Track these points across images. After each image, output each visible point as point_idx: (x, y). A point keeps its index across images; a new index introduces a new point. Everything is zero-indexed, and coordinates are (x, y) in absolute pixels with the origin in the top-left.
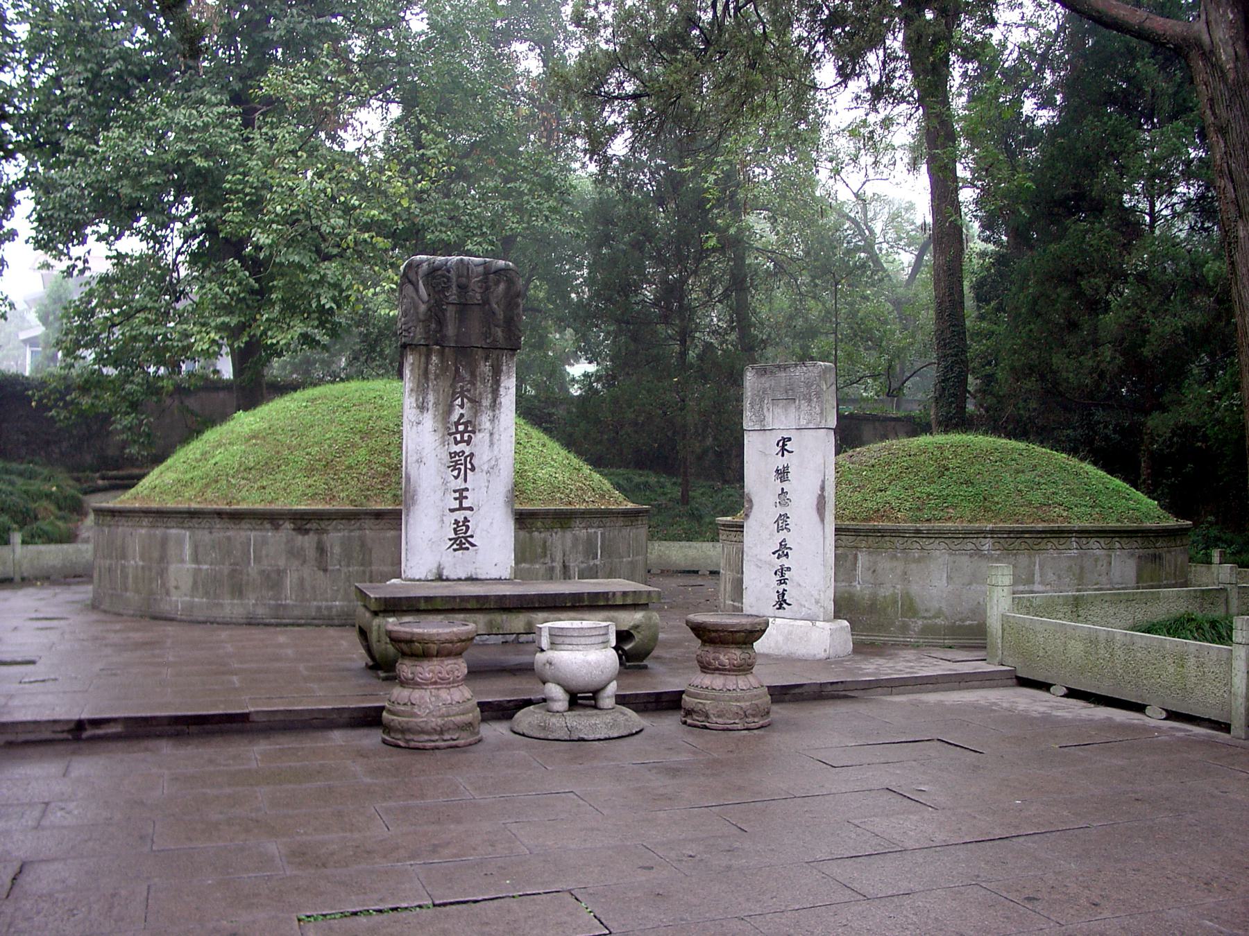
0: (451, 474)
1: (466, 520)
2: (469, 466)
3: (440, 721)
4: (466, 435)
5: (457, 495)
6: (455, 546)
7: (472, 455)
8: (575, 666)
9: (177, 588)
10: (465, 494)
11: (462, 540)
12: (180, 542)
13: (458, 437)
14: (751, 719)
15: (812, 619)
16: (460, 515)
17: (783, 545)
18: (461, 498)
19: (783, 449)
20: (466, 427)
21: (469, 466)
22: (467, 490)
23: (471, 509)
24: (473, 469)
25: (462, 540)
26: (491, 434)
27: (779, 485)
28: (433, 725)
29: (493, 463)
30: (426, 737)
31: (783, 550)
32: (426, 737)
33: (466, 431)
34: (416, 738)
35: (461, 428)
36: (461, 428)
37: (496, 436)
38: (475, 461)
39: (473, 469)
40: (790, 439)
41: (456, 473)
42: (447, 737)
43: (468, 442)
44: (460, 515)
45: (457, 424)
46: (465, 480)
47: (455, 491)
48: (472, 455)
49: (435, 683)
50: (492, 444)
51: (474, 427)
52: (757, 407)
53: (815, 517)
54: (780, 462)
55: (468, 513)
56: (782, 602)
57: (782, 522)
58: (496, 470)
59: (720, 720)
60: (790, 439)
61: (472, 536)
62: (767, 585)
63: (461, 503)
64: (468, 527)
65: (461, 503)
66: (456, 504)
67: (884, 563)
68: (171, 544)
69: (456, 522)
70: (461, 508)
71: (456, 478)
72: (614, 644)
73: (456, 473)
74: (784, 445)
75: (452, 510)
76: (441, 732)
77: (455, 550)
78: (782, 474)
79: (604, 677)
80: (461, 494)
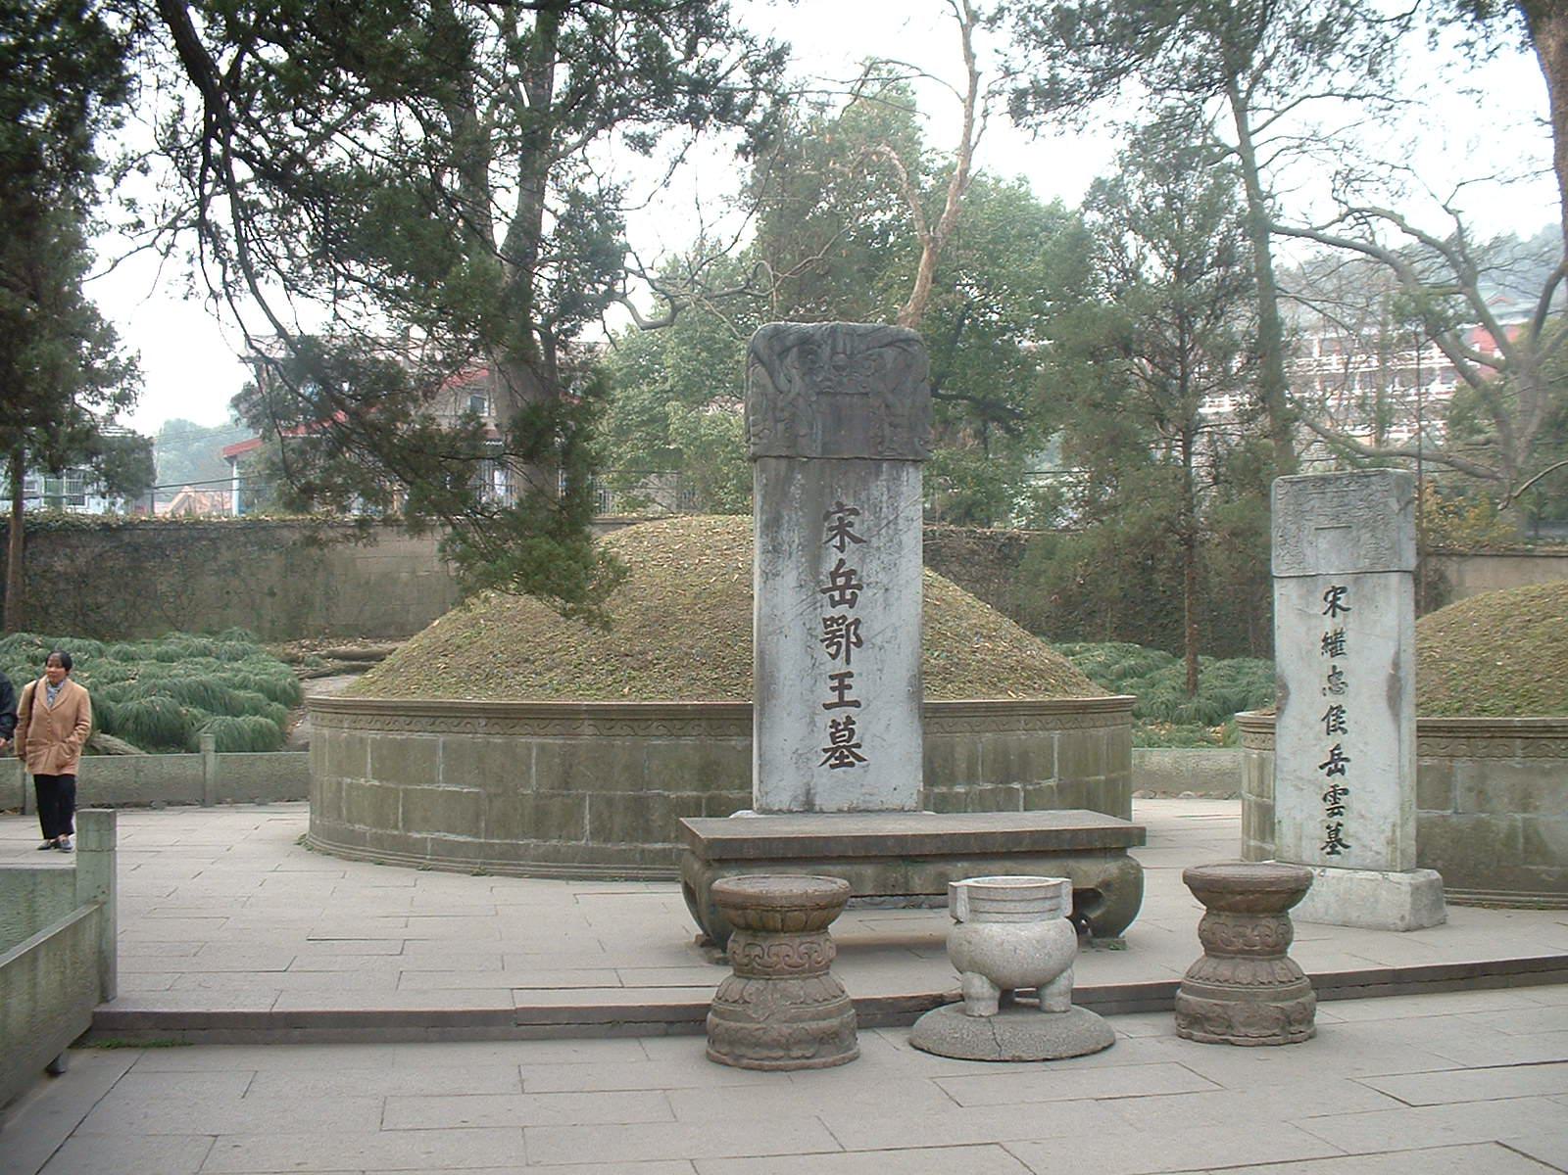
0: (823, 652)
1: (849, 721)
2: (853, 639)
3: (786, 1029)
5: (836, 683)
6: (833, 761)
7: (857, 622)
10: (847, 681)
11: (843, 752)
13: (837, 595)
16: (840, 715)
18: (842, 688)
19: (1334, 605)
21: (853, 639)
22: (850, 675)
23: (856, 704)
27: (1327, 662)
28: (775, 1034)
30: (765, 1053)
31: (1336, 763)
33: (848, 586)
34: (750, 1053)
35: (841, 581)
36: (841, 581)
39: (859, 643)
40: (1343, 590)
41: (833, 650)
42: (796, 1052)
43: (852, 603)
44: (840, 715)
45: (834, 575)
46: (848, 661)
47: (832, 677)
48: (857, 622)
54: (1328, 625)
55: (852, 711)
57: (1335, 719)
59: (1252, 1032)
61: (858, 746)
64: (852, 732)
66: (834, 698)
70: (842, 703)
71: (834, 657)
73: (833, 650)
74: (1336, 599)
75: (827, 707)
76: (787, 1048)
78: (1333, 644)
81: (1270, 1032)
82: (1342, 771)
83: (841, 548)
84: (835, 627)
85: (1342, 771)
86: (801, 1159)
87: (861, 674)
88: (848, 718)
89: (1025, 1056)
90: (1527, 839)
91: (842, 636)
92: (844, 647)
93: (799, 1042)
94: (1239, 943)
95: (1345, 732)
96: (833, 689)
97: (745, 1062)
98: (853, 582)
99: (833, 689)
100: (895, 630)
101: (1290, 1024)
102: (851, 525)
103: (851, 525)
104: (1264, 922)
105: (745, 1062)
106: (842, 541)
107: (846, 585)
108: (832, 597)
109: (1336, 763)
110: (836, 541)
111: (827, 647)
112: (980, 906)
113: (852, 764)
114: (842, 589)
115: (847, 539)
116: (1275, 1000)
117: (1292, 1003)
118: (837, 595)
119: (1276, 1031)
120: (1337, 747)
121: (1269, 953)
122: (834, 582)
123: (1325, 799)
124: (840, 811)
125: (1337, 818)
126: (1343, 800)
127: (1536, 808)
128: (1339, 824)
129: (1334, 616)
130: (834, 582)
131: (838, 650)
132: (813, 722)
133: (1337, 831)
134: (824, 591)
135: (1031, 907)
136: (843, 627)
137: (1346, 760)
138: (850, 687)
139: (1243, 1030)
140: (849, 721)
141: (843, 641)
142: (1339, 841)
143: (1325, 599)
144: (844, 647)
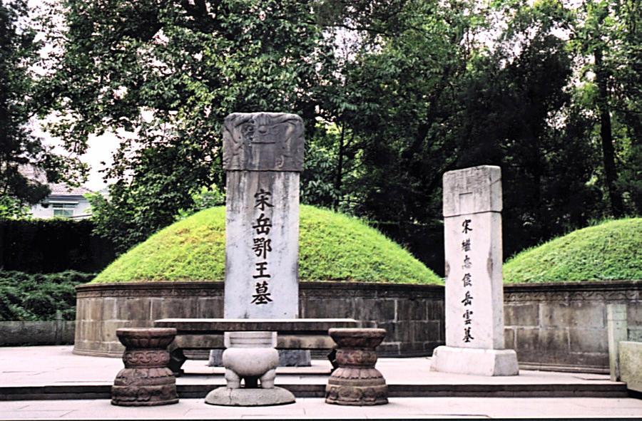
0: (254, 254)
1: (265, 283)
2: (267, 248)
3: (136, 388)
5: (259, 267)
6: (257, 301)
7: (269, 241)
8: (245, 361)
9: (108, 335)
10: (264, 266)
11: (262, 296)
12: (112, 306)
13: (260, 229)
14: (368, 399)
15: (485, 348)
16: (261, 281)
17: (468, 296)
18: (262, 269)
19: (466, 228)
20: (266, 222)
21: (267, 248)
22: (266, 263)
23: (268, 276)
24: (270, 250)
25: (262, 296)
26: (283, 227)
27: (465, 253)
28: (131, 390)
29: (283, 246)
30: (127, 399)
31: (467, 300)
32: (127, 399)
33: (265, 225)
34: (122, 399)
35: (262, 223)
36: (262, 223)
37: (285, 228)
38: (271, 245)
39: (270, 250)
40: (470, 221)
41: (258, 252)
42: (140, 399)
43: (267, 232)
44: (261, 281)
45: (259, 220)
46: (265, 257)
47: (258, 264)
48: (269, 241)
50: (283, 233)
51: (271, 222)
52: (451, 200)
53: (486, 274)
54: (465, 237)
56: (468, 337)
57: (467, 279)
58: (285, 251)
59: (345, 399)
60: (470, 221)
61: (269, 294)
62: (459, 325)
63: (261, 272)
64: (266, 289)
65: (261, 272)
66: (258, 273)
67: (558, 312)
68: (106, 307)
69: (258, 285)
70: (262, 276)
71: (259, 255)
72: (275, 345)
73: (258, 252)
74: (467, 225)
75: (255, 277)
76: (137, 396)
77: (257, 303)
78: (466, 245)
79: (262, 367)
80: (262, 267)
82: (470, 303)
83: (263, 209)
84: (259, 243)
85: (470, 303)
86: (46, 412)
87: (270, 263)
89: (240, 404)
90: (572, 338)
92: (263, 252)
93: (142, 394)
94: (346, 360)
95: (471, 285)
96: (258, 269)
97: (120, 403)
98: (268, 223)
99: (258, 269)
100: (286, 244)
101: (366, 397)
102: (267, 199)
103: (267, 199)
104: (357, 351)
105: (120, 403)
106: (263, 206)
107: (264, 225)
108: (258, 230)
109: (467, 300)
110: (260, 206)
112: (234, 341)
113: (266, 303)
114: (263, 226)
115: (265, 205)
116: (357, 385)
117: (366, 387)
118: (260, 229)
119: (358, 399)
120: (468, 292)
121: (359, 365)
122: (259, 223)
123: (464, 316)
124: (464, 374)
125: (469, 325)
126: (471, 317)
127: (576, 324)
128: (469, 328)
130: (259, 223)
132: (248, 284)
133: (469, 331)
134: (254, 227)
135: (254, 341)
137: (472, 298)
138: (265, 269)
139: (342, 398)
140: (265, 283)
141: (263, 249)
142: (469, 336)
143: (463, 225)
144: (263, 252)
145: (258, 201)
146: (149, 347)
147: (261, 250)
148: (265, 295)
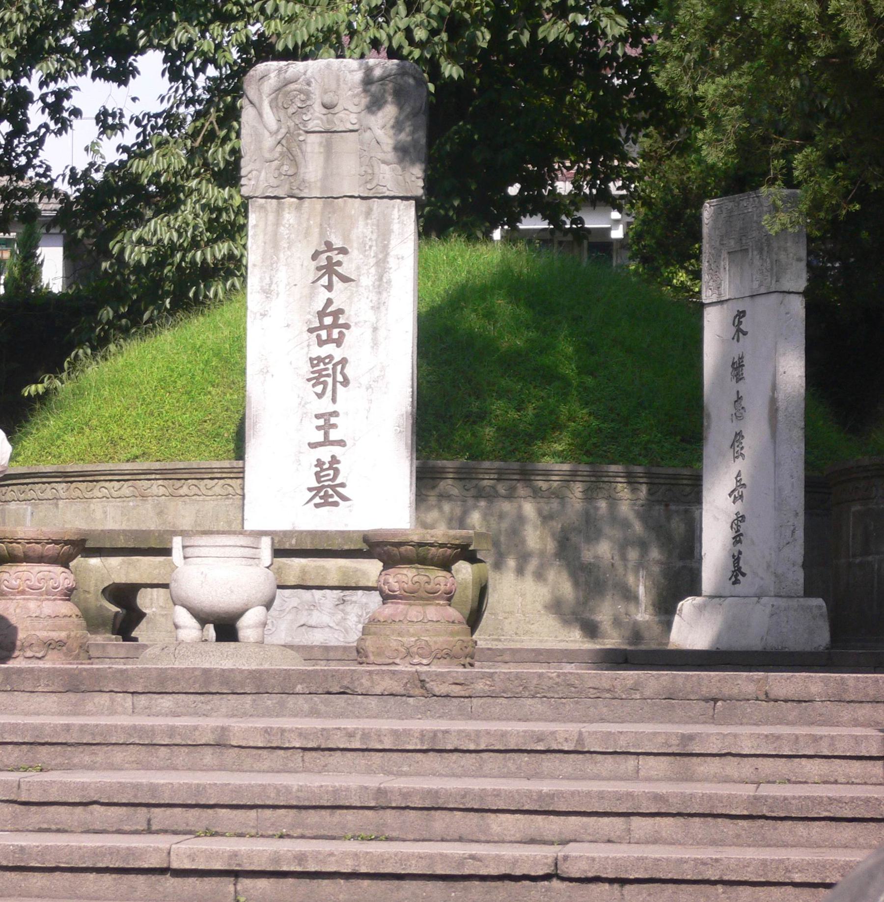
4: (335, 333)
6: (317, 500)
21: (340, 378)
35: (328, 321)
36: (328, 321)
43: (339, 342)
46: (334, 400)
48: (344, 362)
49: (23, 592)
77: (317, 506)
81: (391, 661)
88: (333, 457)
91: (328, 376)
102: (339, 263)
103: (339, 263)
111: (314, 386)
113: (336, 504)
115: (335, 279)
129: (738, 341)
131: (324, 389)
133: (738, 559)
136: (330, 366)
140: (334, 460)
141: (330, 380)
145: (319, 269)
146: (40, 559)
147: (325, 384)
148: (333, 487)
